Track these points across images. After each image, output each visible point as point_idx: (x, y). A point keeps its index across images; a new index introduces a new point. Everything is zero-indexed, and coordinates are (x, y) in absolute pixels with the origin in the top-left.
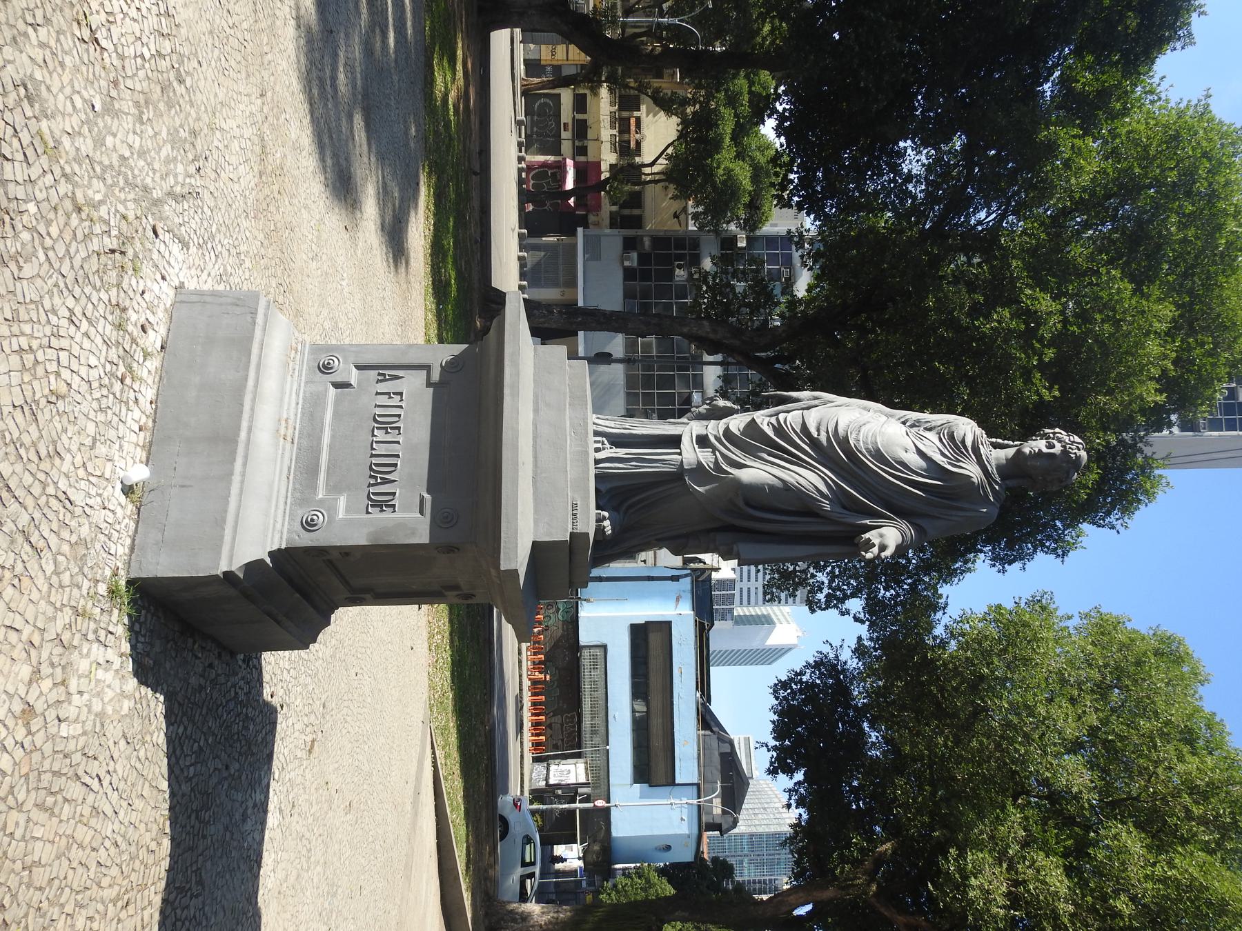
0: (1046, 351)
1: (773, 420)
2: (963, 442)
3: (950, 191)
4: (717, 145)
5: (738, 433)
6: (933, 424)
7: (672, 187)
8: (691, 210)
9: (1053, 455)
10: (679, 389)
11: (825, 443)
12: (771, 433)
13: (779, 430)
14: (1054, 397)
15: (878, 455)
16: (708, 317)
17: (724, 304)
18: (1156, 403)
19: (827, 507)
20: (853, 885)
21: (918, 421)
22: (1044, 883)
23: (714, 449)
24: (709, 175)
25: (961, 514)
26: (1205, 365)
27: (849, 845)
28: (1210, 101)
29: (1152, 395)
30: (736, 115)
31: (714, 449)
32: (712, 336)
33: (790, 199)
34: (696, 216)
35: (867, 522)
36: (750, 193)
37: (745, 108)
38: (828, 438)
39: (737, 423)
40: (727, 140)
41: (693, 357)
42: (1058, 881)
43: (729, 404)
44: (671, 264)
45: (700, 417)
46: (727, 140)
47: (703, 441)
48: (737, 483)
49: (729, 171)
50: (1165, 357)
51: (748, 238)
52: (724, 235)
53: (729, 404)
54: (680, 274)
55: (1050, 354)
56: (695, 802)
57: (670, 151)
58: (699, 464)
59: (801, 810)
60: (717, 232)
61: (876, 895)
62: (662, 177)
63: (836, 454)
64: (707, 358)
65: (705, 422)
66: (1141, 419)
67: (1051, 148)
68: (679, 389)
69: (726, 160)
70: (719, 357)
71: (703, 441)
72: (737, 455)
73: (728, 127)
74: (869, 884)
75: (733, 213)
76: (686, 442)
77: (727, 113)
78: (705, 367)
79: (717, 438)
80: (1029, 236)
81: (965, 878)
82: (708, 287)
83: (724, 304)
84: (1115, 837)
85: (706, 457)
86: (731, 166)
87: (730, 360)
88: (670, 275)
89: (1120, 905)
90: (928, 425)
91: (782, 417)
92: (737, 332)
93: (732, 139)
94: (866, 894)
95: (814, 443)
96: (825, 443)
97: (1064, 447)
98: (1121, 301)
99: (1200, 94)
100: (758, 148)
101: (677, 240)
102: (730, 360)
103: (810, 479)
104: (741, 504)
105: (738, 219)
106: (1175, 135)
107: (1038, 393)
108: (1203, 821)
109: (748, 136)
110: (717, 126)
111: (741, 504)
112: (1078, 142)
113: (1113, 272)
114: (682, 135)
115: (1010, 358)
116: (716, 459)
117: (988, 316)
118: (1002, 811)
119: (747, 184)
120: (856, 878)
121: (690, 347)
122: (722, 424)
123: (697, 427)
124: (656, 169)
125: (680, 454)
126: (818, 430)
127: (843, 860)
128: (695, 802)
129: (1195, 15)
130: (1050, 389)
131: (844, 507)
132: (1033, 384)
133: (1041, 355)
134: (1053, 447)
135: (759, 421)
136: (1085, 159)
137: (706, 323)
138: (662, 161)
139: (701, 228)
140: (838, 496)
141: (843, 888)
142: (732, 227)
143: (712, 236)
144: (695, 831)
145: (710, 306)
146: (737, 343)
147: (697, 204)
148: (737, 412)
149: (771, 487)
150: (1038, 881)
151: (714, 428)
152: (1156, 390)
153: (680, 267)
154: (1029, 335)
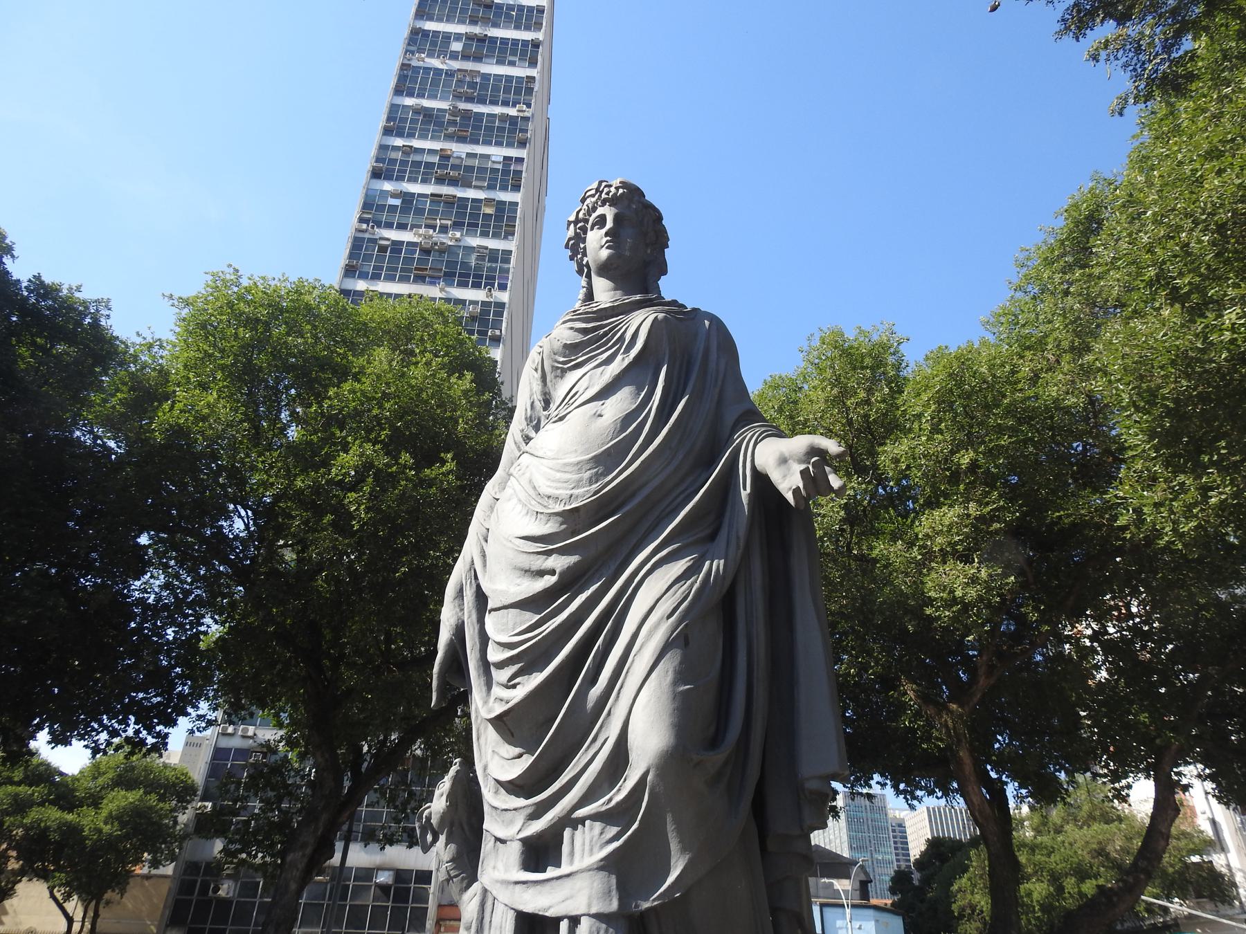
0: (401, 461)
1: (501, 676)
2: (584, 331)
3: (197, 546)
4: (72, 831)
5: (528, 760)
6: (538, 397)
7: (108, 895)
8: (145, 871)
9: (617, 218)
10: (369, 900)
11: (572, 559)
12: (537, 679)
13: (530, 660)
14: (453, 459)
15: (606, 460)
16: (283, 854)
17: (274, 833)
18: (472, 381)
19: (718, 564)
20: (954, 728)
21: (529, 420)
22: (950, 526)
23: (570, 821)
24: (110, 844)
25: (713, 355)
26: (443, 343)
27: (912, 731)
28: (176, 296)
29: (466, 381)
30: (42, 804)
31: (570, 821)
32: (309, 851)
33: (159, 735)
34: (155, 864)
35: (745, 494)
36: (146, 793)
37: (37, 792)
38: (562, 551)
39: (497, 760)
40: (70, 817)
41: (332, 879)
42: (948, 515)
43: (445, 785)
44: (210, 901)
45: (468, 862)
46: (70, 817)
47: (540, 853)
48: (673, 762)
49: (110, 819)
50: (428, 364)
51: (202, 800)
52: (191, 829)
53: (445, 785)
54: (226, 889)
55: (405, 457)
56: (848, 911)
57: (58, 895)
58: (607, 865)
59: (873, 783)
60: (185, 837)
61: (961, 706)
62: (93, 903)
63: (599, 540)
64: (336, 860)
65: (487, 845)
66: (487, 396)
67: (178, 432)
68: (369, 900)
69: (91, 821)
70: (339, 846)
71: (540, 853)
72: (589, 762)
73: (53, 815)
74: (950, 712)
75: (166, 816)
76: (538, 902)
77: (34, 814)
78: (349, 863)
79: (537, 814)
80: (272, 467)
81: (954, 601)
82: (241, 851)
83: (274, 833)
84: (896, 461)
85: (587, 848)
86: (104, 813)
87: (345, 827)
88: (226, 903)
89: (965, 461)
90: (539, 405)
91: (494, 655)
92: (310, 814)
93: (70, 811)
94: (961, 716)
95: (570, 583)
96: (572, 559)
97: (604, 203)
98: (363, 393)
99: (168, 303)
100: (95, 778)
101: (180, 892)
102: (345, 827)
103: (656, 596)
104: (718, 758)
105: (173, 810)
106: (201, 326)
107: (445, 474)
108: (870, 391)
109: (75, 790)
110: (47, 828)
111: (718, 758)
112: (179, 406)
113: (331, 393)
114: (44, 875)
115: (403, 497)
116: (595, 817)
117: (351, 516)
118: (878, 561)
119: (133, 796)
120: (946, 726)
121: (320, 882)
122: (491, 797)
123: (500, 866)
124: (78, 916)
125: (575, 921)
126: (541, 573)
127: (928, 738)
128: (848, 911)
129: (77, 295)
130: (443, 462)
131: (712, 537)
132: (435, 478)
133: (405, 466)
134: (602, 219)
135: (499, 709)
136: (203, 406)
137: (289, 858)
138: (70, 906)
139: (173, 858)
140: (700, 536)
141: (959, 741)
142: (183, 818)
143: (188, 844)
144: (871, 912)
145: (269, 849)
146: (324, 817)
147: (139, 860)
148: (469, 762)
149: (681, 676)
150: (949, 531)
151: (507, 823)
152: (459, 378)
153: (217, 889)
154: (385, 479)
